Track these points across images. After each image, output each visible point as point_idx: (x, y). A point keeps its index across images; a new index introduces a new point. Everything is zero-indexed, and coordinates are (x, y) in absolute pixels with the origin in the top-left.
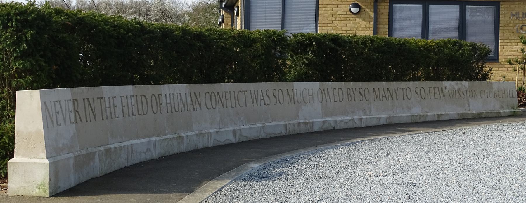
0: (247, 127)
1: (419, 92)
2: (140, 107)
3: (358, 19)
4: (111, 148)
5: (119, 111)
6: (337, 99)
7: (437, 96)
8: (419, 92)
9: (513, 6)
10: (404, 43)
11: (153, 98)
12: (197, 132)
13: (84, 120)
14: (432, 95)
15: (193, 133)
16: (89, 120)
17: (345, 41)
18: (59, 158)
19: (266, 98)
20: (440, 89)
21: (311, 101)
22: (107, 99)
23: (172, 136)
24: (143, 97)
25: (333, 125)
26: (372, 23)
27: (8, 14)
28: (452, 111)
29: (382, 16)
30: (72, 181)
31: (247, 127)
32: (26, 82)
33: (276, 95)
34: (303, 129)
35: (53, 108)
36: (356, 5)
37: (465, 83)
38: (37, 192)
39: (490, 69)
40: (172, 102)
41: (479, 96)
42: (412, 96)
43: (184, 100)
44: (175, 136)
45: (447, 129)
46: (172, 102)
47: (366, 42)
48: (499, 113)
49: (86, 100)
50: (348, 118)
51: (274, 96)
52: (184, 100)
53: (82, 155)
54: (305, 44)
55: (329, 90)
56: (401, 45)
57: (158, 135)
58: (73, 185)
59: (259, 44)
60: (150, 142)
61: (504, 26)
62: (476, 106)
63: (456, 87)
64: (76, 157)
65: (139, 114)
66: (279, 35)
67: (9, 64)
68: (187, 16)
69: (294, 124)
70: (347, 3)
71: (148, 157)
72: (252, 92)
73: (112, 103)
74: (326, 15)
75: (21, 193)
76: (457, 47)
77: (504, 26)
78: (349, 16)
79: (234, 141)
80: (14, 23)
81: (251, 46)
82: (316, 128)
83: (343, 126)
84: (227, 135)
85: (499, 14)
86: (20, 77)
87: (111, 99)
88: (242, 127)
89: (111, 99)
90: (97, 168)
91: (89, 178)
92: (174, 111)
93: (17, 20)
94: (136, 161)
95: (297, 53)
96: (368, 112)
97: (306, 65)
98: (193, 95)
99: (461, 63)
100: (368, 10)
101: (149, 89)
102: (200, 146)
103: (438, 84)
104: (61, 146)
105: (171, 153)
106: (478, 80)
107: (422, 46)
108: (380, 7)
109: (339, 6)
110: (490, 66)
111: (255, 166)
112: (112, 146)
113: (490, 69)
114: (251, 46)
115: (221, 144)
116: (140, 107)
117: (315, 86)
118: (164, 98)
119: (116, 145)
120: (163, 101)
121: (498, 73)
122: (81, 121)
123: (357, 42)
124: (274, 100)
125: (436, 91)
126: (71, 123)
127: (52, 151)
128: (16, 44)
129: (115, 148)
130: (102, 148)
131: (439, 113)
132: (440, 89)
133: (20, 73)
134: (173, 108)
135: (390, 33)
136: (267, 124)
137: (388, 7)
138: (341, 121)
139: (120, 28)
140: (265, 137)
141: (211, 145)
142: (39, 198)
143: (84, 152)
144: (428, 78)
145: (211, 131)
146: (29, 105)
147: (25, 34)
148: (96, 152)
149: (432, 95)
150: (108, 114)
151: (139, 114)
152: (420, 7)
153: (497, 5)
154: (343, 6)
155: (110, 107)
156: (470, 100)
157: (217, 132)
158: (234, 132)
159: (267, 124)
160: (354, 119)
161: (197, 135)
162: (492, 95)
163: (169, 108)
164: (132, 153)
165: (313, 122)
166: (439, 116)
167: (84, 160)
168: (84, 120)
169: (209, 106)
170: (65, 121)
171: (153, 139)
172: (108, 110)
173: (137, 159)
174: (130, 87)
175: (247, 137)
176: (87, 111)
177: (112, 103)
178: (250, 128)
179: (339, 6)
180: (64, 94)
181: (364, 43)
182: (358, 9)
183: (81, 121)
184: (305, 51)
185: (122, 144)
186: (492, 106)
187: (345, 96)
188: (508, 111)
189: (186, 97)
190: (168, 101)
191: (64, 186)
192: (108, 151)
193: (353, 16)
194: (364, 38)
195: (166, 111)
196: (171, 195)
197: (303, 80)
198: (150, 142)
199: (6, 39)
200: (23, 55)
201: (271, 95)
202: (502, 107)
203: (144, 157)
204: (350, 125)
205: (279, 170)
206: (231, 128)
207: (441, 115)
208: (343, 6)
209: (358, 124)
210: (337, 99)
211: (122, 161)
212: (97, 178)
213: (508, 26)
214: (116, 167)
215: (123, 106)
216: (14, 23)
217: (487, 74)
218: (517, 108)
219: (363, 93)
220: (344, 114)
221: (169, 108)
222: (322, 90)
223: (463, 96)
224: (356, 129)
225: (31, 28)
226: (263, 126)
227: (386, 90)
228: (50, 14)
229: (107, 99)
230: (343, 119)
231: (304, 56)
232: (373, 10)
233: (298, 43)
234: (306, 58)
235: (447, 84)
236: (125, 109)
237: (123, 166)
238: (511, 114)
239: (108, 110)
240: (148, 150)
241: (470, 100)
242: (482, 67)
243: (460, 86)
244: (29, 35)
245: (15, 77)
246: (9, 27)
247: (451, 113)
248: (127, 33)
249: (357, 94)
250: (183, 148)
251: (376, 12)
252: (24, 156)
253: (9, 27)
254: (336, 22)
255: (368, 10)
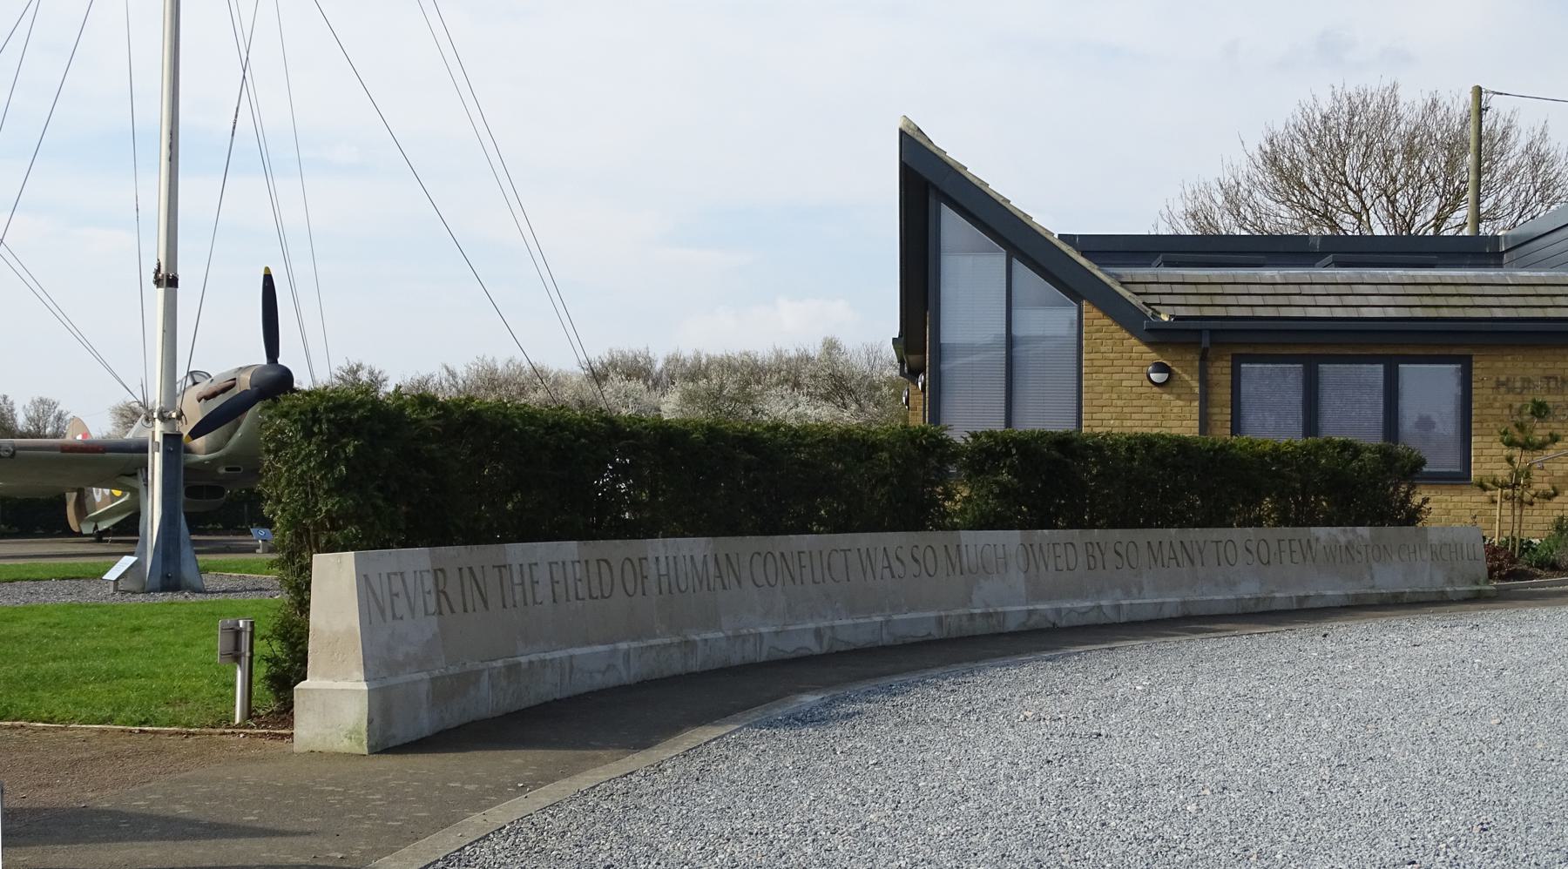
0: (850, 622)
1: (1254, 550)
2: (595, 583)
3: (1166, 397)
4: (520, 664)
5: (543, 591)
6: (1062, 564)
7: (1297, 557)
8: (1254, 550)
9: (1500, 365)
10: (1222, 448)
11: (628, 566)
12: (730, 633)
13: (458, 608)
14: (1286, 557)
15: (721, 635)
16: (470, 607)
17: (1088, 446)
18: (392, 681)
19: (896, 565)
20: (1304, 542)
21: (1002, 566)
22: (516, 568)
23: (667, 641)
24: (603, 564)
25: (1052, 618)
26: (1197, 403)
27: (314, 410)
28: (1333, 589)
29: (1217, 390)
30: (426, 724)
31: (850, 622)
32: (346, 538)
33: (919, 557)
34: (981, 627)
35: (386, 586)
36: (1160, 368)
37: (1364, 531)
38: (345, 745)
39: (1426, 501)
40: (672, 573)
41: (1395, 558)
42: (1239, 557)
43: (700, 568)
44: (676, 640)
45: (1297, 627)
46: (672, 573)
47: (1182, 444)
48: (1443, 592)
49: (466, 572)
50: (1088, 604)
51: (916, 561)
52: (700, 568)
53: (450, 676)
54: (989, 454)
55: (1045, 548)
56: (1216, 452)
57: (638, 638)
58: (426, 733)
59: (885, 455)
60: (615, 651)
61: (1482, 407)
62: (1388, 579)
63: (1343, 540)
64: (433, 680)
65: (591, 597)
66: (931, 436)
67: (316, 504)
68: (885, 389)
69: (959, 616)
70: (1141, 363)
71: (611, 680)
72: (863, 551)
73: (527, 577)
74: (1100, 389)
75: (318, 746)
76: (1346, 455)
77: (1482, 407)
78: (1147, 388)
79: (816, 650)
80: (324, 427)
81: (869, 458)
82: (1012, 625)
83: (1076, 620)
84: (802, 636)
85: (1470, 382)
86: (333, 528)
87: (526, 569)
88: (837, 622)
89: (526, 569)
90: (486, 701)
91: (465, 720)
92: (675, 590)
93: (329, 421)
94: (582, 688)
95: (982, 471)
96: (1135, 591)
97: (997, 496)
98: (722, 559)
99: (1365, 489)
100: (1187, 377)
101: (616, 550)
102: (736, 660)
103: (1301, 532)
104: (400, 657)
105: (666, 674)
106: (1401, 523)
107: (1265, 454)
108: (1212, 371)
109: (1127, 369)
110: (1425, 494)
111: (810, 699)
112: (523, 659)
113: (1426, 501)
114: (869, 458)
115: (786, 656)
116: (595, 583)
117: (1010, 539)
118: (653, 566)
119: (534, 657)
120: (652, 571)
121: (1445, 510)
122: (452, 611)
123: (1114, 448)
124: (914, 568)
125: (1295, 545)
126: (426, 613)
127: (378, 666)
128: (328, 465)
129: (531, 662)
130: (499, 663)
131: (1302, 594)
132: (1304, 542)
133: (334, 521)
134: (674, 585)
135: (1236, 428)
136: (895, 617)
137: (1229, 371)
138: (1071, 610)
139: (562, 429)
140: (891, 642)
141: (763, 658)
142: (349, 756)
143: (453, 670)
144: (1284, 521)
145: (763, 630)
146: (335, 577)
147: (344, 447)
148: (479, 673)
149: (1286, 557)
150: (518, 597)
151: (591, 597)
152: (1294, 371)
153: (1466, 364)
154: (1133, 369)
155: (522, 584)
156: (1375, 565)
157: (777, 633)
158: (818, 633)
159: (895, 617)
160: (1100, 607)
161: (728, 638)
162: (1426, 555)
163: (665, 586)
164: (571, 671)
165: (1004, 613)
166: (1300, 599)
167: (443, 690)
168: (458, 608)
169: (761, 580)
170: (412, 610)
171: (623, 646)
172: (518, 589)
173: (581, 685)
174: (573, 544)
175: (848, 643)
176: (468, 593)
177: (527, 577)
178: (856, 626)
179: (1127, 369)
180: (417, 559)
181: (1131, 449)
182: (1166, 376)
183: (452, 611)
184: (996, 470)
185: (548, 656)
186: (1428, 578)
187: (1082, 558)
188: (1465, 588)
189: (705, 563)
190: (663, 571)
191: (402, 734)
192: (513, 669)
193: (1156, 389)
194: (1129, 439)
195: (656, 591)
196: (601, 753)
197: (992, 527)
198: (615, 651)
199: (310, 455)
200: (341, 487)
201: (908, 559)
202: (1451, 582)
203: (599, 681)
204: (1092, 618)
205: (852, 708)
206: (811, 625)
207: (1307, 597)
208: (1133, 369)
209: (1112, 617)
210: (1062, 564)
211: (547, 688)
212: (485, 720)
213: (1491, 406)
214: (530, 700)
215: (553, 582)
216: (324, 427)
217: (1418, 509)
218: (1487, 582)
219: (1123, 552)
220: (1080, 594)
221: (665, 586)
222: (1027, 548)
223: (1358, 557)
224: (1105, 626)
225: (357, 435)
226: (888, 622)
227: (1177, 547)
228: (402, 408)
229: (516, 568)
230: (1077, 606)
231: (991, 478)
232: (1197, 376)
233: (982, 450)
234: (996, 482)
235: (1321, 532)
236: (560, 589)
237: (550, 698)
238: (1469, 595)
239: (518, 589)
240: (610, 667)
241: (1375, 565)
242: (1408, 494)
243: (1351, 536)
244: (350, 449)
245: (323, 527)
246: (314, 434)
247: (1330, 593)
248: (578, 438)
249: (1110, 555)
250: (695, 664)
251: (1204, 382)
252: (325, 676)
253: (314, 434)
254: (1120, 403)
255: (1187, 377)
